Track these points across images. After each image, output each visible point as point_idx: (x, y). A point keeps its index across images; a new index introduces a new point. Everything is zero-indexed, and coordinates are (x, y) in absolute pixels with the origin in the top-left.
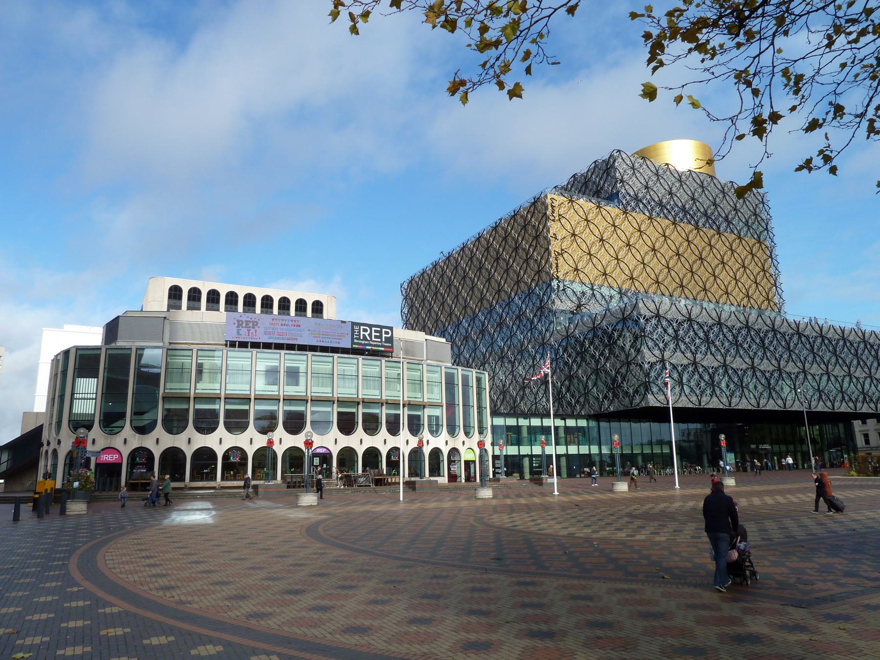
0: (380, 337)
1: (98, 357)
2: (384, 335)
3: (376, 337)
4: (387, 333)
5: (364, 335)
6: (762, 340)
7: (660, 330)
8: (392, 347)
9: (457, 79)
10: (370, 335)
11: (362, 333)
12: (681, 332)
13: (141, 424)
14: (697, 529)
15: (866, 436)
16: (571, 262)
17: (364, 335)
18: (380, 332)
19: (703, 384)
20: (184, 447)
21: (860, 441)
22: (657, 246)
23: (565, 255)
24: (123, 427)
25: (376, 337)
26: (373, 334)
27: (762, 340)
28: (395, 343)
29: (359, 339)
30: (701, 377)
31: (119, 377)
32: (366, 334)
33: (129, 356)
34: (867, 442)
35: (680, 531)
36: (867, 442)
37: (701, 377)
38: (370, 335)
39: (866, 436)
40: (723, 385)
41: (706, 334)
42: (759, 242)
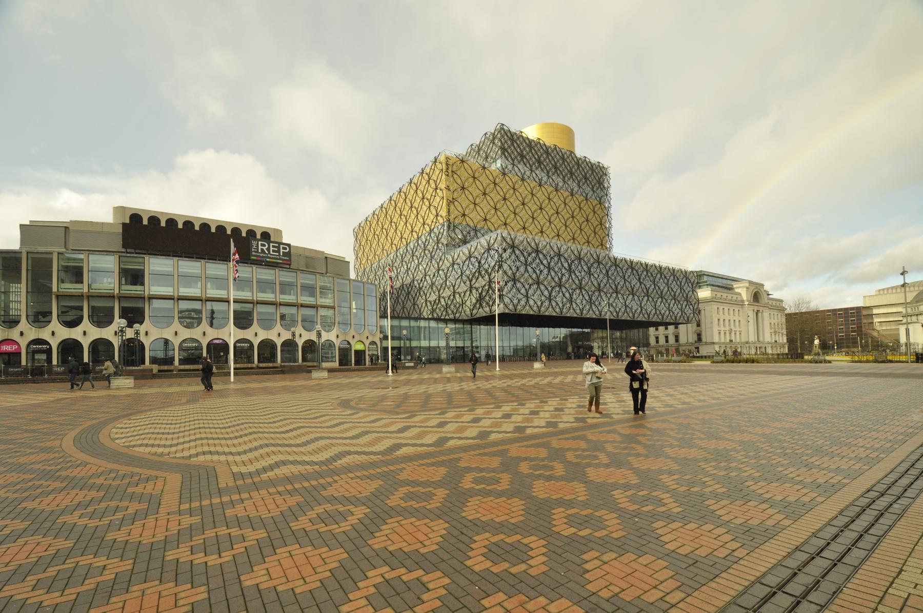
0: (279, 251)
1: (19, 260)
2: (282, 250)
3: (274, 251)
4: (284, 248)
5: (262, 250)
6: (607, 272)
7: (538, 261)
8: (290, 260)
9: (704, 293)
10: (268, 249)
11: (260, 247)
12: (552, 264)
13: (69, 318)
14: (579, 406)
15: (657, 338)
16: (460, 209)
17: (262, 250)
18: (279, 248)
19: (584, 302)
20: (80, 338)
21: (652, 341)
22: (511, 191)
23: (456, 203)
24: (19, 322)
25: (274, 251)
26: (271, 249)
27: (607, 272)
28: (293, 258)
29: (257, 252)
30: (564, 295)
31: (575, 330)
32: (265, 248)
33: (51, 261)
34: (657, 342)
35: (561, 410)
36: (657, 342)
37: (564, 295)
38: (268, 249)
39: (657, 338)
40: (578, 301)
41: (570, 266)
42: (600, 204)
